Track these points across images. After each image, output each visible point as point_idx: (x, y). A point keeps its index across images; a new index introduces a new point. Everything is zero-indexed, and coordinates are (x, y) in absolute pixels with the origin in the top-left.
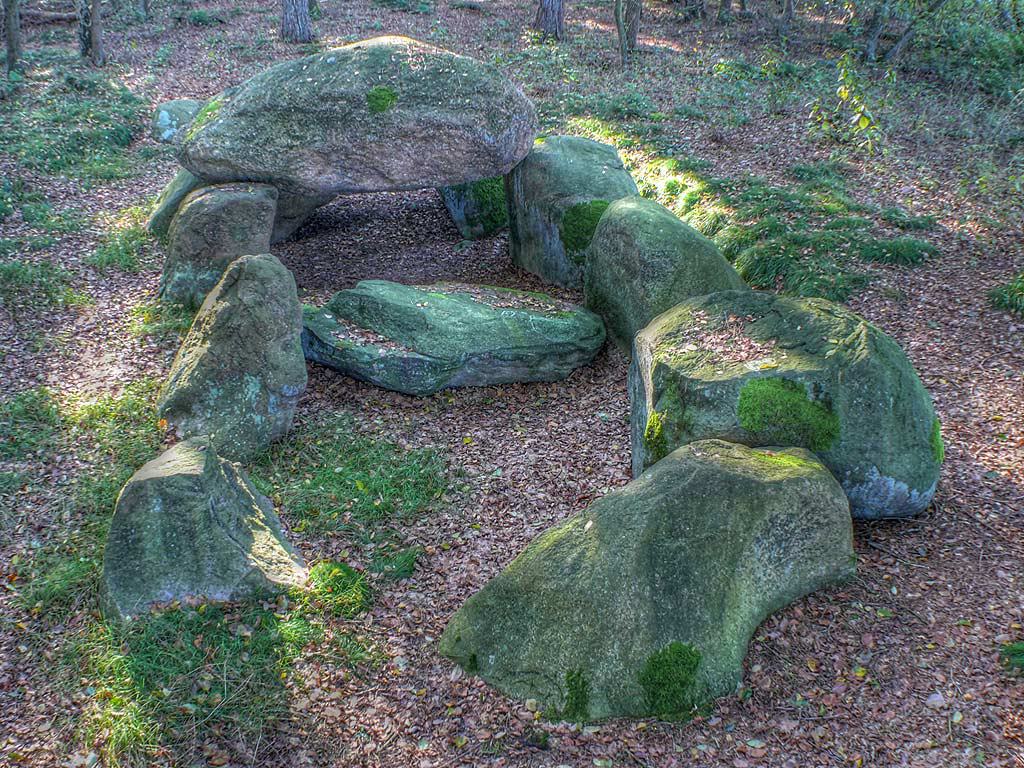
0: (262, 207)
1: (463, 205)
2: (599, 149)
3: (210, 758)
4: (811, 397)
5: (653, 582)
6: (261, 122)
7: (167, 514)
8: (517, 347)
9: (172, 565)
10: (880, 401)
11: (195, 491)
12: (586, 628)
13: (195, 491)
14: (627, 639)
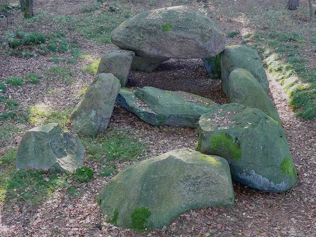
0: (127, 59)
1: (210, 66)
2: (250, 51)
3: (14, 209)
4: (234, 141)
5: (142, 187)
6: (132, 31)
7: (36, 142)
8: (187, 115)
9: (36, 157)
10: (257, 147)
11: (45, 137)
12: (122, 197)
13: (45, 137)
14: (130, 202)
